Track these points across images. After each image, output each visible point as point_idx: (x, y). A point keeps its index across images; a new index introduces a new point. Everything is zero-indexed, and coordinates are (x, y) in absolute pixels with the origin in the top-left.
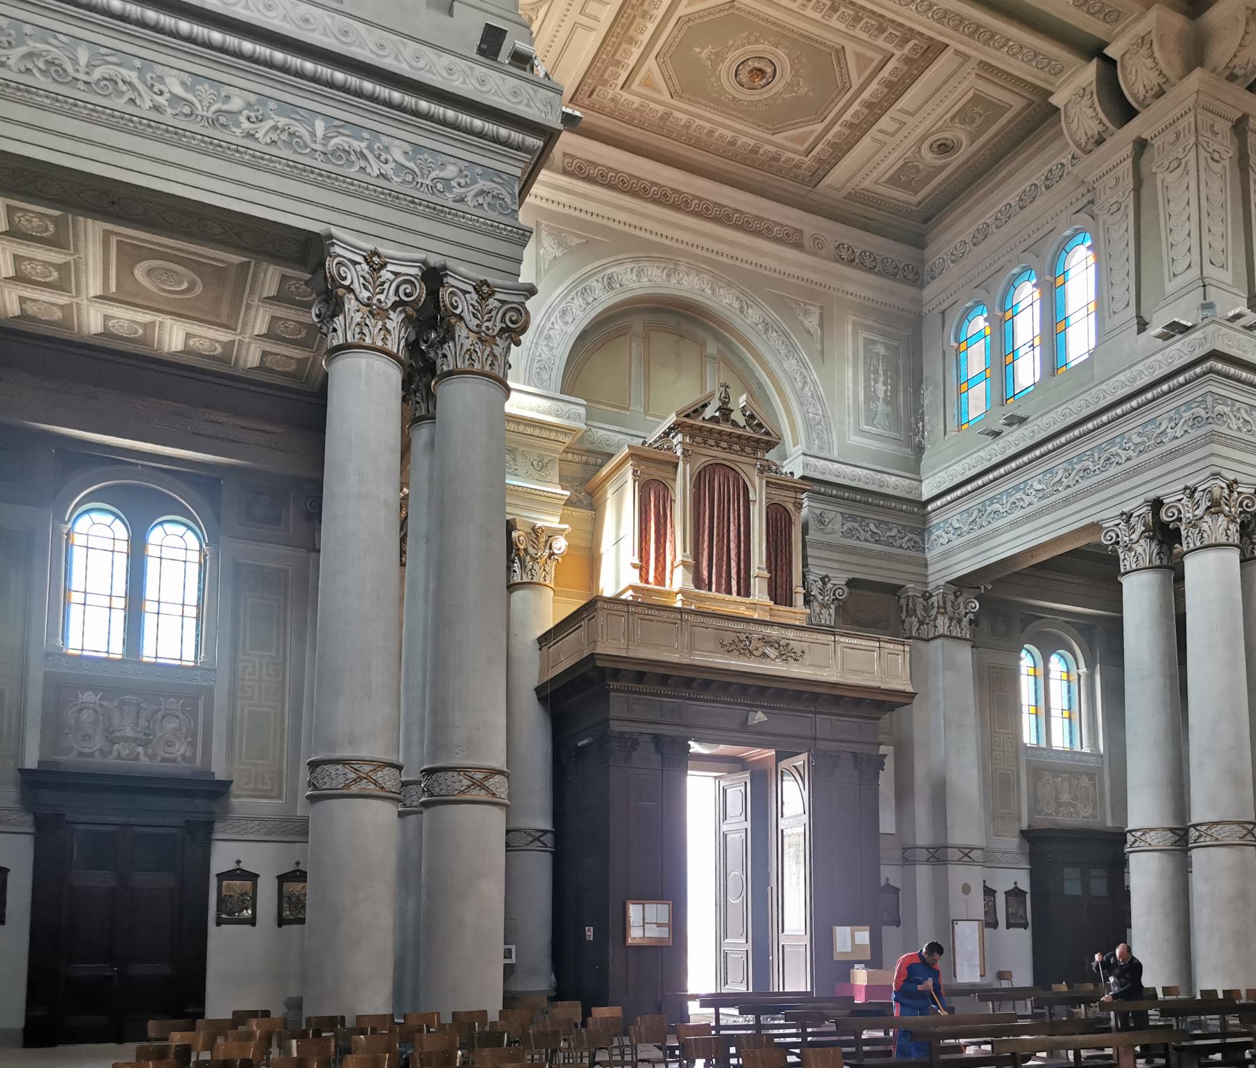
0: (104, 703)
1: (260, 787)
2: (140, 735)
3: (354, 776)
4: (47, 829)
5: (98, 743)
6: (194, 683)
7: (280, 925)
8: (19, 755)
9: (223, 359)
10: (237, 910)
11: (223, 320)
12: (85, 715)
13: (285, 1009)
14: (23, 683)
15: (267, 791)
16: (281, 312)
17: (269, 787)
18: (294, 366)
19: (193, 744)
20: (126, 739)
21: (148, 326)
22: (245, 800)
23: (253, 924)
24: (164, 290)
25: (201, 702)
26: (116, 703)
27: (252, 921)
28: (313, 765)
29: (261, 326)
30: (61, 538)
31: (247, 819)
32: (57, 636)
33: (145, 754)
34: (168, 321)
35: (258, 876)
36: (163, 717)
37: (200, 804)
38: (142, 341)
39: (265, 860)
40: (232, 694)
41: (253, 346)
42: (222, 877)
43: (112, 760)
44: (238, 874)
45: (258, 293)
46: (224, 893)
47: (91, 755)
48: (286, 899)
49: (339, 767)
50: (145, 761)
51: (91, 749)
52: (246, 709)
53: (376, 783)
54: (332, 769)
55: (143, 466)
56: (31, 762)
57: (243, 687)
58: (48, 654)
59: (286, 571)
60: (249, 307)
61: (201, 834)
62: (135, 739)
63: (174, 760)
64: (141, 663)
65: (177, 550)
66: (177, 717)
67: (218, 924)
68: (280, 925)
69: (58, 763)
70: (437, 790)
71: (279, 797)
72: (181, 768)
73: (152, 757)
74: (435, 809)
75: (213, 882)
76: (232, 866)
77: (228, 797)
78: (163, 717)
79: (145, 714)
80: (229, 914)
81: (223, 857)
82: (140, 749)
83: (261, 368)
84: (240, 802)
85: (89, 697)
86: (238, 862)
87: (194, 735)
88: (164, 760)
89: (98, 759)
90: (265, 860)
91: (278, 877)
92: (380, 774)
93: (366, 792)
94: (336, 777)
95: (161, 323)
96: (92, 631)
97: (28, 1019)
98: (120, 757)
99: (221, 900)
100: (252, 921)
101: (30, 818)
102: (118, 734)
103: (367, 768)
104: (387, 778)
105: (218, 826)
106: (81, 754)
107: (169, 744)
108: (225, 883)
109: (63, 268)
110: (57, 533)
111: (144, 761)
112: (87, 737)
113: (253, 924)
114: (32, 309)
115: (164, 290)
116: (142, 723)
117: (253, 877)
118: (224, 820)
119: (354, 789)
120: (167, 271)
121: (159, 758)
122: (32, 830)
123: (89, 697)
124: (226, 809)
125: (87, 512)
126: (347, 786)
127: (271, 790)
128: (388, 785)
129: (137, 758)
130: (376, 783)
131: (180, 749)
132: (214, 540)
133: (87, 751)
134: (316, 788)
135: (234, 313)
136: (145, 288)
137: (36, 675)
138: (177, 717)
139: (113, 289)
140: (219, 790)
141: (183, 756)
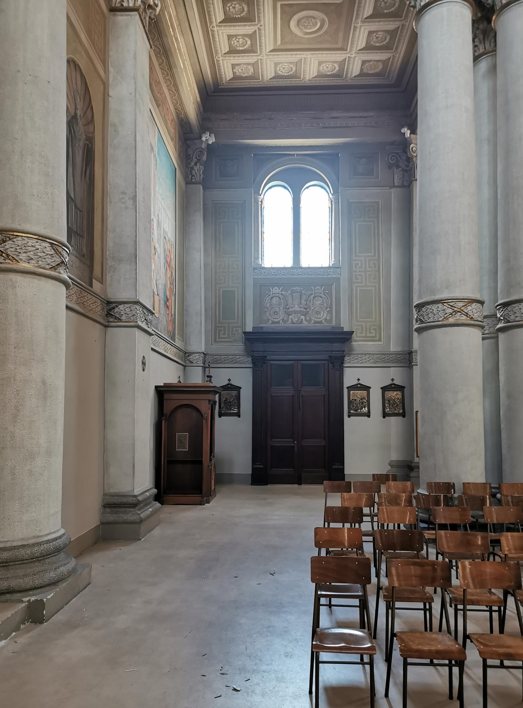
0: (283, 293)
1: (368, 335)
2: (302, 309)
3: (450, 311)
4: (258, 363)
5: (282, 315)
6: (329, 276)
7: (384, 417)
8: (244, 324)
9: (338, 75)
10: (361, 409)
11: (339, 45)
12: (274, 300)
13: (389, 468)
14: (244, 287)
15: (372, 337)
16: (374, 26)
17: (374, 335)
18: (381, 67)
19: (330, 312)
20: (296, 312)
21: (297, 64)
22: (360, 343)
23: (369, 416)
24: (306, 33)
25: (334, 286)
26: (289, 292)
27: (238, 415)
28: (420, 306)
29: (361, 43)
30: (258, 204)
31: (362, 354)
32: (258, 258)
33: (306, 320)
34: (308, 55)
35: (370, 388)
36: (314, 298)
37: (336, 346)
38: (295, 76)
39: (375, 378)
40: (351, 282)
41: (357, 58)
42: (350, 388)
43: (289, 324)
44: (359, 387)
45: (360, 17)
46: (351, 398)
47: (279, 322)
48: (387, 402)
49: (440, 305)
50: (307, 324)
51: (279, 320)
52: (358, 289)
53: (467, 315)
54: (434, 307)
55: (297, 155)
56: (249, 328)
57: (356, 275)
58: (254, 269)
59: (378, 203)
60: (355, 27)
61: (337, 363)
62: (300, 312)
63: (320, 322)
64: (302, 268)
65: (317, 200)
66: (321, 297)
67: (349, 416)
68: (384, 417)
69: (262, 327)
70: (512, 317)
71: (380, 340)
72: (325, 326)
73: (309, 321)
74: (510, 332)
75: (346, 391)
76: (356, 382)
77: (351, 342)
78: (314, 298)
79: (304, 297)
80: (355, 411)
81: (350, 377)
82: (303, 317)
83: (362, 74)
84: (359, 344)
85: (276, 290)
86: (359, 380)
87: (331, 307)
88: (316, 322)
89: (282, 324)
90: (375, 378)
91: (381, 388)
92: (469, 308)
93: (460, 322)
94: (436, 313)
95: (305, 58)
96: (275, 252)
97: (253, 469)
98: (293, 323)
99: (350, 402)
100: (238, 415)
101: (250, 359)
102: (291, 310)
103: (460, 304)
104: (473, 310)
105: (346, 358)
106: (273, 323)
107: (318, 313)
108: (351, 392)
109: (252, 36)
110: (256, 202)
111: (305, 323)
112: (276, 313)
113: (369, 416)
114: (239, 71)
115: (306, 33)
116: (303, 302)
117: (367, 388)
118: (349, 355)
119: (451, 320)
120: (308, 17)
121: (313, 322)
122: (251, 366)
123: (276, 290)
124: (351, 349)
125: (270, 188)
126: (446, 318)
127: (375, 337)
128: (475, 316)
129: (301, 322)
130: (467, 315)
131: (324, 316)
132: (336, 192)
133: (276, 320)
134: (422, 322)
135: (346, 38)
136: (296, 36)
137: (249, 282)
138: (321, 297)
139: (279, 42)
140: (345, 338)
141: (326, 319)
